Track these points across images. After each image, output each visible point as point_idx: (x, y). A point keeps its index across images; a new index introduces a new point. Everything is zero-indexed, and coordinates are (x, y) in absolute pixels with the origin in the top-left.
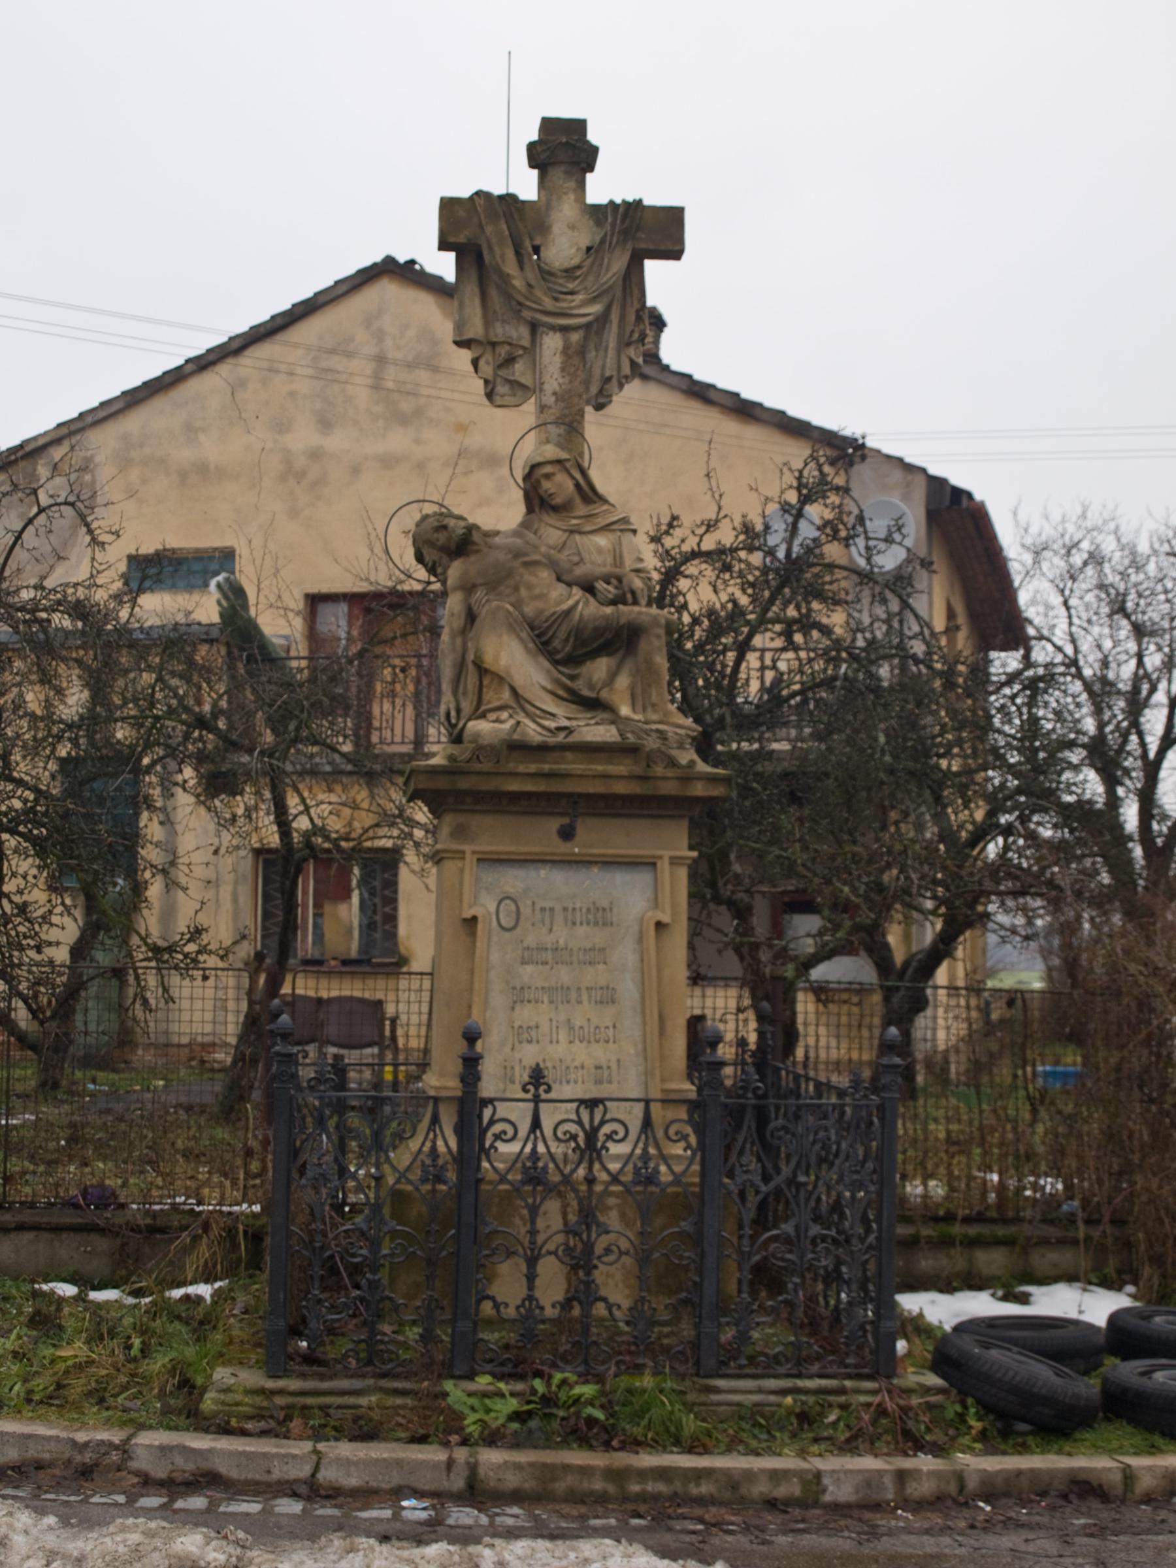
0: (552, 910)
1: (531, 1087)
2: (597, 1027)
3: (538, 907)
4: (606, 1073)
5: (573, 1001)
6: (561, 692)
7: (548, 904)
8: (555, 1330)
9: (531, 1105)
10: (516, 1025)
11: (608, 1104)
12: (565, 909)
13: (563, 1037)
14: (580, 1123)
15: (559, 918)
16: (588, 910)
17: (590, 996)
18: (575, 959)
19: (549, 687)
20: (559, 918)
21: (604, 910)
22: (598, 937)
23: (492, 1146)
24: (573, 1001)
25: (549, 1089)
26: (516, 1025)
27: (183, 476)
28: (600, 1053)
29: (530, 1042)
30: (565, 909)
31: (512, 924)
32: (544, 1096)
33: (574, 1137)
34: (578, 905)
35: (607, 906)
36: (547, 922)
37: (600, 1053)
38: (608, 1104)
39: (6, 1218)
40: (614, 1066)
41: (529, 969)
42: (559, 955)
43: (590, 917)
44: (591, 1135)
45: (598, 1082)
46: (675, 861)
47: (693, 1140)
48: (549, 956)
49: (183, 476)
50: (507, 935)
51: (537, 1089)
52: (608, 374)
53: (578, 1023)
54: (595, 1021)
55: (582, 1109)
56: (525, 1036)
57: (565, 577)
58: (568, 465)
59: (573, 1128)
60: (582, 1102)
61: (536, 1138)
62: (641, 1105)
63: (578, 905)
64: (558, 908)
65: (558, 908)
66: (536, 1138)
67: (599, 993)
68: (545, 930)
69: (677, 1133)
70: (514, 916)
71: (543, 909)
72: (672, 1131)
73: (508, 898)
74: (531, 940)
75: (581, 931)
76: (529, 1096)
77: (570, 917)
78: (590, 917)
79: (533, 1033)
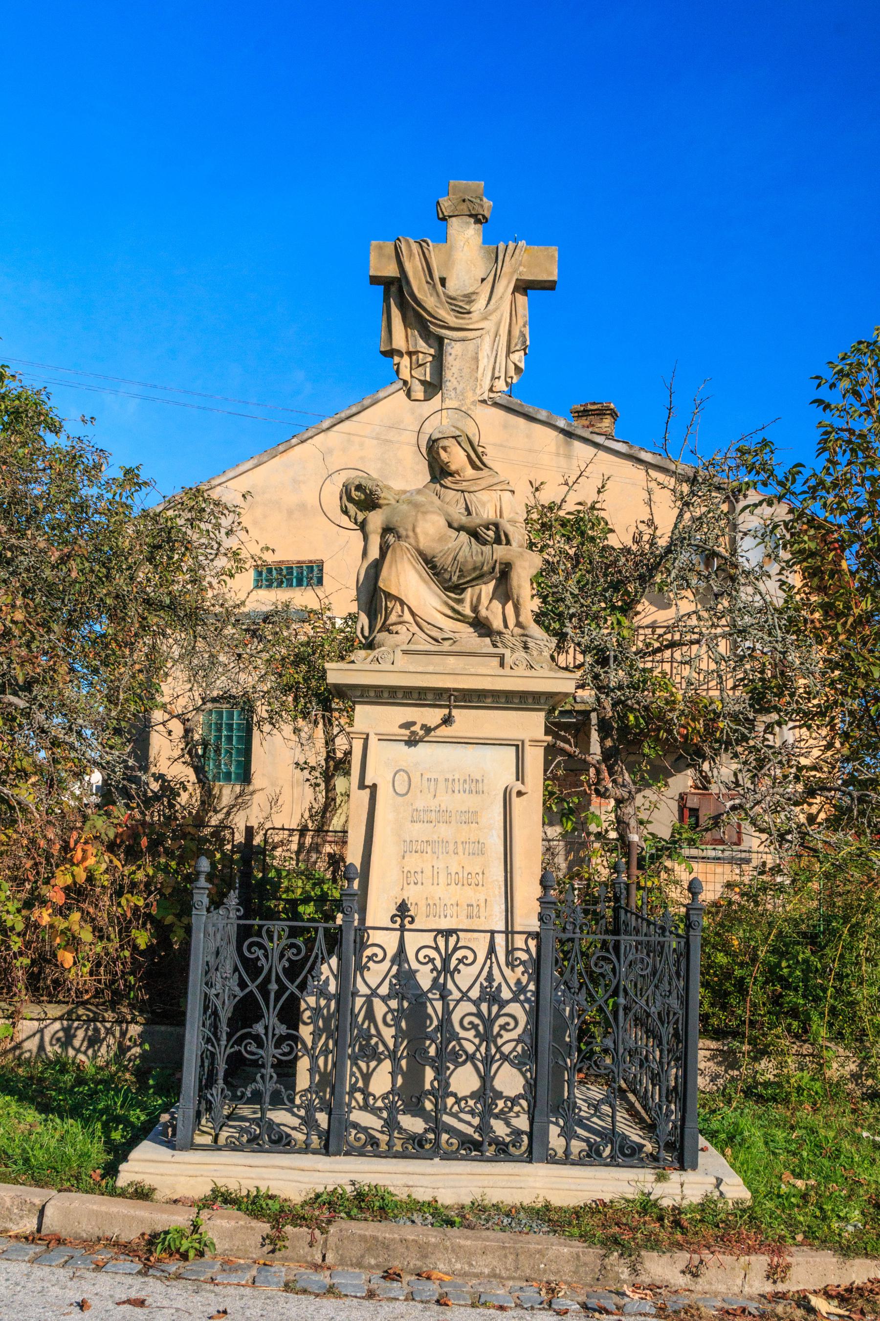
0: (436, 780)
1: (398, 919)
3: (425, 777)
4: (476, 910)
5: (451, 852)
6: (449, 613)
9: (399, 933)
10: (405, 870)
11: (460, 934)
13: (443, 879)
14: (437, 949)
15: (442, 785)
16: (465, 781)
17: (464, 849)
18: (453, 818)
19: (439, 608)
20: (442, 785)
21: (477, 781)
22: (469, 802)
23: (456, 969)
24: (451, 852)
26: (405, 870)
27: (290, 513)
28: (469, 895)
29: (416, 884)
30: (447, 780)
32: (408, 926)
33: (432, 960)
34: (456, 777)
36: (432, 790)
37: (469, 895)
38: (460, 934)
40: (482, 904)
41: (418, 826)
42: (443, 816)
43: (467, 786)
44: (446, 961)
45: (470, 916)
46: (535, 742)
49: (290, 513)
50: (400, 799)
51: (402, 920)
52: (497, 375)
53: (453, 871)
54: (468, 869)
55: (439, 938)
56: (412, 880)
57: (455, 525)
58: (459, 439)
59: (433, 954)
60: (439, 932)
61: (492, 963)
63: (456, 777)
64: (441, 779)
65: (441, 779)
66: (492, 963)
67: (472, 846)
68: (430, 796)
70: (406, 783)
71: (429, 780)
72: (421, 956)
73: (407, 772)
74: (420, 804)
75: (457, 796)
76: (397, 926)
77: (450, 786)
78: (467, 786)
79: (419, 876)
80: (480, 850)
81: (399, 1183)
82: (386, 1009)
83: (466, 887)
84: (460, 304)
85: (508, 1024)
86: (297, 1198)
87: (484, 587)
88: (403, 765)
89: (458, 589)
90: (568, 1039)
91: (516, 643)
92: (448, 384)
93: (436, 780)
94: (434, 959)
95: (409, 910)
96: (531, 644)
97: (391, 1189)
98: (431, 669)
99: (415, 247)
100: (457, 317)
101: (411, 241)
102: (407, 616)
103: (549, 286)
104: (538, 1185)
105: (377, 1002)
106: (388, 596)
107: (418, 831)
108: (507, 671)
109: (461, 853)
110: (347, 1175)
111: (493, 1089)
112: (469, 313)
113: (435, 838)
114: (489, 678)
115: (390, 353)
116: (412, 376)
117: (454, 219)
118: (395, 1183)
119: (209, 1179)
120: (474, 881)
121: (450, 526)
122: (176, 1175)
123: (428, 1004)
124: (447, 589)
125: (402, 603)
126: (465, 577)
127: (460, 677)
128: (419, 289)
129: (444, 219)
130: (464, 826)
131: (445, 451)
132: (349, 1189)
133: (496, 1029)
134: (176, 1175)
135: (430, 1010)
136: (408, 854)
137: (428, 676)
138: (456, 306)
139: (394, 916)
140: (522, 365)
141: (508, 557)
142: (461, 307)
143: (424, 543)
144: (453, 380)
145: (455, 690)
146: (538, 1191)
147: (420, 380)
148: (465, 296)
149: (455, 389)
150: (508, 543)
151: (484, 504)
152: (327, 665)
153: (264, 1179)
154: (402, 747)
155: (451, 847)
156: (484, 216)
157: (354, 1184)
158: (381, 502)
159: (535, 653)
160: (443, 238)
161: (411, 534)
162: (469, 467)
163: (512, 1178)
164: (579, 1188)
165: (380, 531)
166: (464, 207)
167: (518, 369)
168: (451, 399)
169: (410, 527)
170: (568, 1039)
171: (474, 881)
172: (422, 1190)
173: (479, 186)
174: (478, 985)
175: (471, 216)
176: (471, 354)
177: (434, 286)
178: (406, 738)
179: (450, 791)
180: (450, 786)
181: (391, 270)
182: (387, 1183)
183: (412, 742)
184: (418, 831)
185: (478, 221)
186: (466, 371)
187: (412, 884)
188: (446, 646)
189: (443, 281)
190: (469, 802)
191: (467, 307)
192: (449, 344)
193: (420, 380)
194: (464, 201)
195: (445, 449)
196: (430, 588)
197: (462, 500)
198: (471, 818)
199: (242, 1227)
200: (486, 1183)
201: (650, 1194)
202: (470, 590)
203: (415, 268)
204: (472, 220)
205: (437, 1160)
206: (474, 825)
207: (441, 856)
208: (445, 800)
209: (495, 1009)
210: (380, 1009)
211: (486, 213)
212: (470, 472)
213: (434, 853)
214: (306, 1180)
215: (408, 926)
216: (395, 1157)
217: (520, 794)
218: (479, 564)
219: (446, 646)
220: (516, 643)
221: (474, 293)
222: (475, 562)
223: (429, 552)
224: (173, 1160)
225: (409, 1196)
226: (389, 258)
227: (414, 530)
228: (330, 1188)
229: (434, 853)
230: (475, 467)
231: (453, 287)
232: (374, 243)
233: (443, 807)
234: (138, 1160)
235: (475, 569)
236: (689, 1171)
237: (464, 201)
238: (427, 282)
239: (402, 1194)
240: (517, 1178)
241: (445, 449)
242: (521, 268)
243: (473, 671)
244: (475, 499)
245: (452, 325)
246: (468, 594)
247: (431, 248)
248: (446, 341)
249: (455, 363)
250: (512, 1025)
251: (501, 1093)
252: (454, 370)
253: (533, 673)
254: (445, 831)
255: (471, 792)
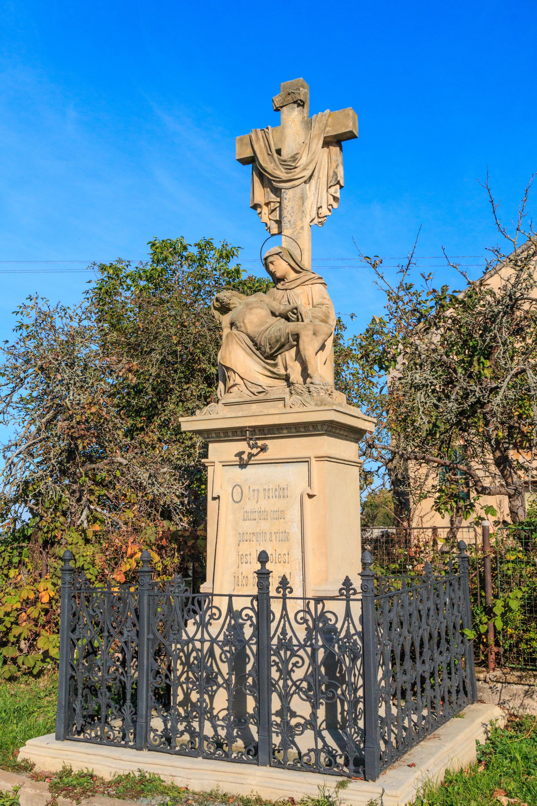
0: (258, 490)
2: (242, 555)
3: (251, 489)
5: (268, 540)
6: (269, 374)
7: (256, 488)
8: (183, 715)
10: (240, 554)
12: (265, 490)
15: (262, 493)
16: (276, 489)
17: (276, 537)
18: (269, 516)
20: (262, 493)
21: (284, 489)
22: (277, 504)
24: (268, 540)
25: (291, 592)
29: (246, 563)
30: (265, 490)
31: (239, 500)
32: (288, 595)
34: (271, 487)
35: (285, 487)
36: (256, 497)
39: (535, 673)
41: (247, 523)
42: (263, 515)
47: (254, 620)
48: (256, 515)
50: (236, 505)
54: (278, 552)
56: (244, 560)
62: (227, 598)
64: (261, 489)
65: (261, 489)
68: (255, 501)
69: (301, 619)
70: (240, 494)
71: (254, 490)
73: (240, 487)
74: (248, 508)
75: (272, 500)
76: (280, 595)
77: (267, 494)
78: (277, 493)
79: (248, 557)
80: (285, 537)
81: (168, 773)
82: (220, 651)
83: (278, 564)
84: (289, 163)
85: (298, 662)
86: (108, 778)
87: (287, 353)
88: (238, 481)
89: (272, 357)
90: (338, 675)
91: (304, 389)
92: (285, 219)
93: (258, 490)
94: (252, 617)
95: (351, 584)
96: (312, 389)
97: (162, 777)
98: (240, 414)
99: (260, 134)
100: (287, 173)
101: (259, 130)
102: (238, 380)
103: (350, 136)
104: (254, 782)
105: (216, 648)
106: (228, 369)
107: (248, 526)
108: (288, 410)
109: (274, 541)
110: (137, 764)
111: (289, 710)
112: (296, 168)
113: (258, 531)
114: (277, 416)
115: (255, 207)
116: (270, 219)
117: (284, 108)
118: (165, 772)
119: (61, 761)
120: (282, 560)
121: (273, 314)
122: (45, 756)
123: (247, 647)
124: (267, 358)
125: (234, 372)
126: (274, 348)
127: (259, 418)
128: (263, 160)
129: (277, 110)
130: (276, 521)
131: (273, 264)
132: (137, 774)
133: (290, 666)
134: (45, 756)
135: (248, 651)
136: (241, 543)
137: (239, 419)
138: (287, 165)
139: (341, 589)
140: (338, 195)
141: (296, 329)
142: (290, 166)
143: (251, 329)
144: (288, 215)
145: (249, 427)
146: (254, 788)
147: (275, 221)
148: (292, 157)
149: (290, 221)
150: (303, 321)
151: (298, 296)
152: (181, 419)
153: (91, 763)
154: (237, 469)
155: (268, 536)
156: (301, 101)
157: (140, 771)
158: (231, 306)
159: (315, 395)
160: (277, 123)
161: (242, 324)
162: (292, 272)
163: (239, 775)
164: (281, 787)
165: (229, 325)
166: (289, 98)
167: (335, 199)
168: (287, 229)
169: (241, 320)
170: (338, 675)
171: (282, 560)
172: (180, 779)
173: (299, 81)
174: (222, 633)
175: (295, 102)
176: (298, 195)
177: (272, 156)
178: (238, 463)
179: (267, 497)
180: (267, 494)
181: (248, 153)
182: (160, 772)
183: (243, 465)
184: (248, 526)
185: (299, 105)
186: (296, 207)
187: (244, 563)
188: (261, 396)
189: (279, 152)
190: (277, 504)
191: (293, 164)
192: (285, 192)
193: (275, 221)
194: (289, 94)
195: (272, 263)
196: (253, 359)
197: (286, 296)
198: (280, 515)
199: (38, 794)
200: (220, 778)
201: (330, 797)
202: (279, 356)
203: (260, 147)
204: (296, 105)
205: (200, 759)
206: (282, 520)
207: (261, 543)
208: (264, 504)
209: (289, 653)
210: (217, 651)
211: (302, 98)
212: (293, 275)
213: (257, 541)
214: (114, 766)
215: (288, 595)
216: (175, 754)
217: (310, 496)
218: (278, 338)
219: (261, 396)
220: (304, 389)
221: (297, 154)
222: (276, 337)
223: (252, 334)
224: (47, 746)
225: (172, 783)
226: (247, 145)
227: (243, 322)
228: (126, 773)
229: (257, 541)
230: (297, 272)
231: (286, 154)
232: (238, 138)
233: (263, 509)
234: (30, 745)
235: (277, 341)
236: (371, 782)
237: (289, 94)
238: (269, 155)
239: (168, 781)
240: (242, 776)
241: (272, 263)
242: (328, 129)
243: (266, 412)
244: (293, 293)
245: (284, 179)
246: (279, 359)
247: (270, 131)
248: (283, 190)
249: (289, 204)
250: (301, 662)
251: (295, 713)
252: (289, 209)
253: (305, 409)
254: (264, 526)
255: (280, 497)
